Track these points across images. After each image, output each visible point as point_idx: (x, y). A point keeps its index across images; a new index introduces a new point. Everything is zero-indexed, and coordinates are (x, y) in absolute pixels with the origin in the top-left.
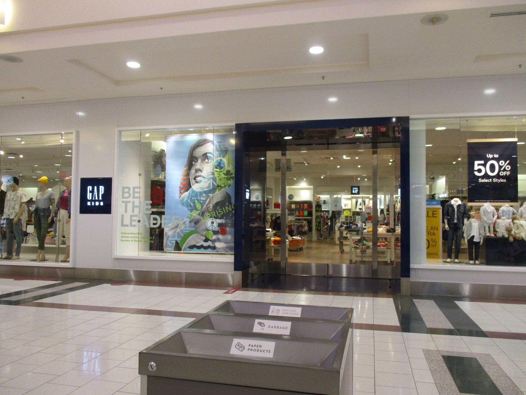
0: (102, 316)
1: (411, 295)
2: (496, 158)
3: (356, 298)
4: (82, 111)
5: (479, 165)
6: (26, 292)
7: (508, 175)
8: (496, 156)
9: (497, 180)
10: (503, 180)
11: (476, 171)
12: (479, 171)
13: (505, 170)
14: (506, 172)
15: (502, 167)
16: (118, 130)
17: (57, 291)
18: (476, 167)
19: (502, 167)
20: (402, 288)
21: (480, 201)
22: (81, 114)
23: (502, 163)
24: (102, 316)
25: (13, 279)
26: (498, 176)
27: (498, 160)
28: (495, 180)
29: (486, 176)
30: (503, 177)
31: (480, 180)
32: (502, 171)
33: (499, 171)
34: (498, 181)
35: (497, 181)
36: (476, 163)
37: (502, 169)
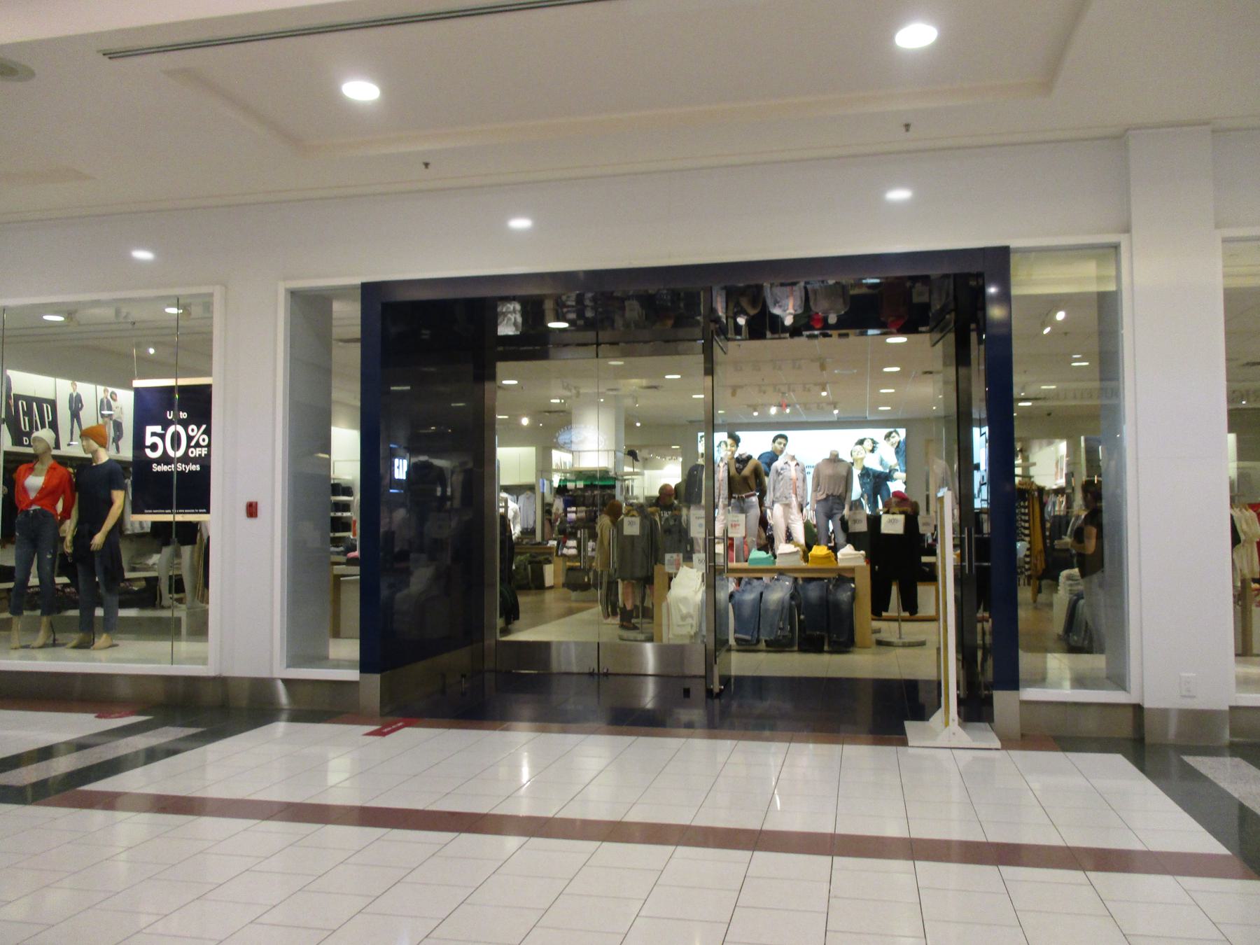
0: (167, 832)
1: (1022, 735)
2: (183, 419)
3: (795, 747)
4: (901, 184)
5: (154, 434)
6: (46, 753)
7: (203, 455)
8: (183, 415)
9: (183, 466)
10: (194, 466)
11: (148, 447)
12: (154, 447)
13: (198, 445)
14: (200, 449)
15: (193, 437)
16: (287, 290)
17: (158, 745)
18: (149, 440)
19: (193, 437)
20: (995, 717)
21: (154, 511)
22: (143, 255)
23: (193, 430)
24: (167, 832)
25: (94, 713)
26: (185, 459)
27: (185, 423)
28: (181, 467)
29: (165, 459)
30: (195, 461)
31: (157, 468)
32: (192, 447)
33: (188, 446)
34: (185, 468)
35: (184, 470)
36: (150, 429)
37: (193, 443)
